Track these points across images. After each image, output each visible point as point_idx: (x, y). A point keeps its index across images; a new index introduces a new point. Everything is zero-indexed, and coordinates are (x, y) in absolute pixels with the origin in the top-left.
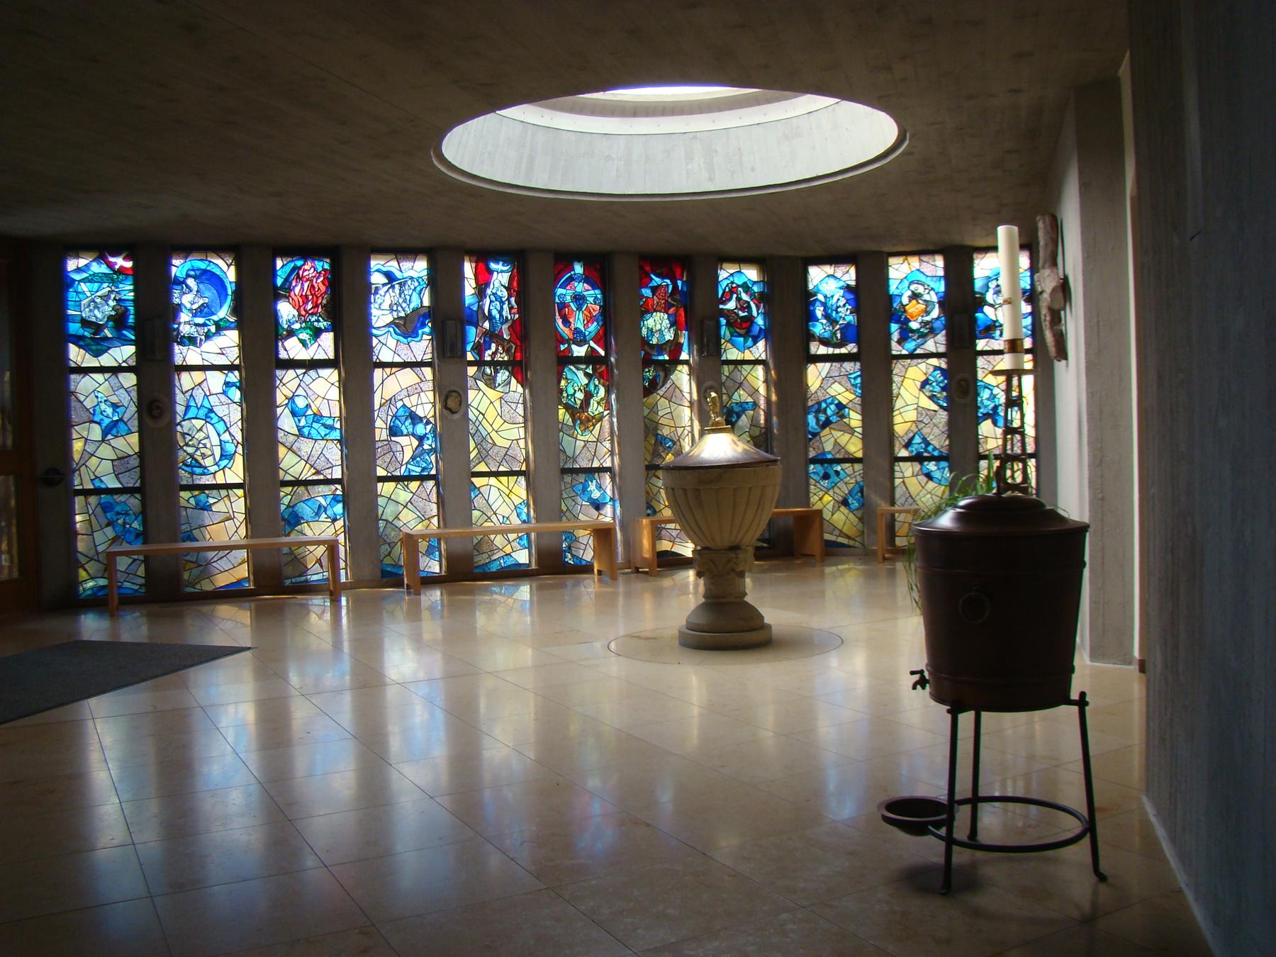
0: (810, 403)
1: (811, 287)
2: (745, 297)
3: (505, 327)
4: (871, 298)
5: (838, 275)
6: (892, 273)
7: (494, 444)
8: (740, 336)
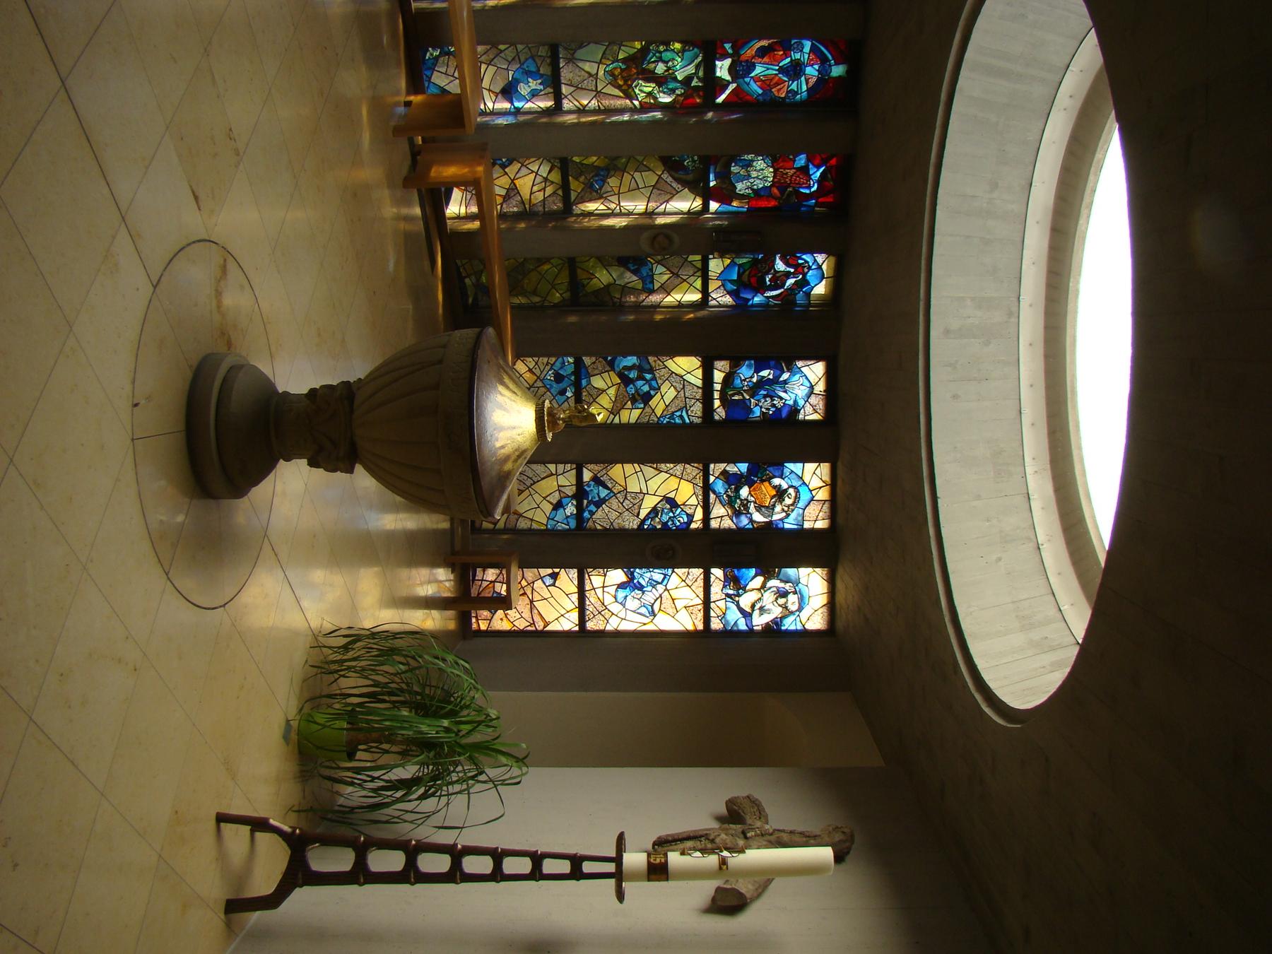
0: (651, 359)
1: (800, 364)
2: (790, 281)
4: (781, 440)
5: (813, 400)
6: (810, 467)
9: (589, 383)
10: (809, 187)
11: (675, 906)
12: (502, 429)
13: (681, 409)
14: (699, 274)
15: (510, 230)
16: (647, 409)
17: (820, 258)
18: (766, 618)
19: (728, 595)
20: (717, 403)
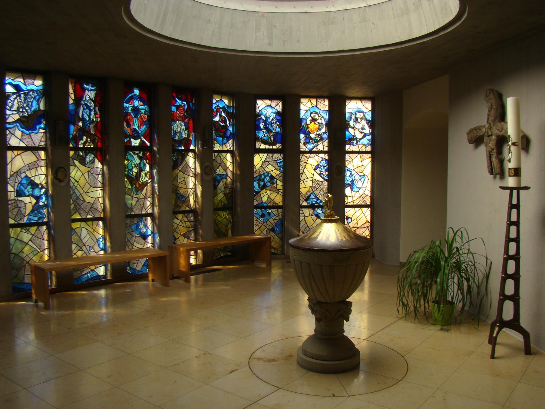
0: (255, 176)
1: (258, 111)
2: (223, 114)
3: (92, 126)
4: (290, 120)
5: (273, 105)
6: (302, 107)
7: (84, 201)
8: (221, 137)
9: (265, 202)
10: (185, 105)
11: (530, 165)
12: (337, 237)
13: (277, 163)
14: (220, 154)
15: (202, 236)
16: (277, 177)
17: (214, 101)
18: (367, 127)
19: (356, 143)
20: (274, 147)
